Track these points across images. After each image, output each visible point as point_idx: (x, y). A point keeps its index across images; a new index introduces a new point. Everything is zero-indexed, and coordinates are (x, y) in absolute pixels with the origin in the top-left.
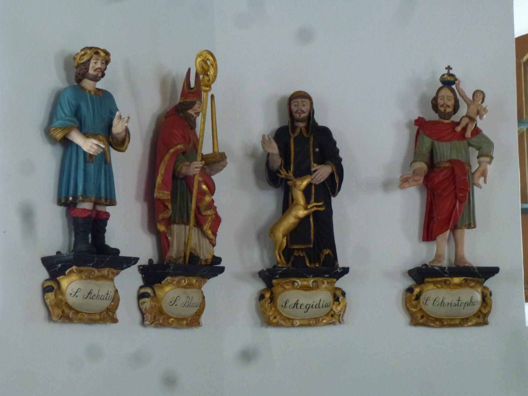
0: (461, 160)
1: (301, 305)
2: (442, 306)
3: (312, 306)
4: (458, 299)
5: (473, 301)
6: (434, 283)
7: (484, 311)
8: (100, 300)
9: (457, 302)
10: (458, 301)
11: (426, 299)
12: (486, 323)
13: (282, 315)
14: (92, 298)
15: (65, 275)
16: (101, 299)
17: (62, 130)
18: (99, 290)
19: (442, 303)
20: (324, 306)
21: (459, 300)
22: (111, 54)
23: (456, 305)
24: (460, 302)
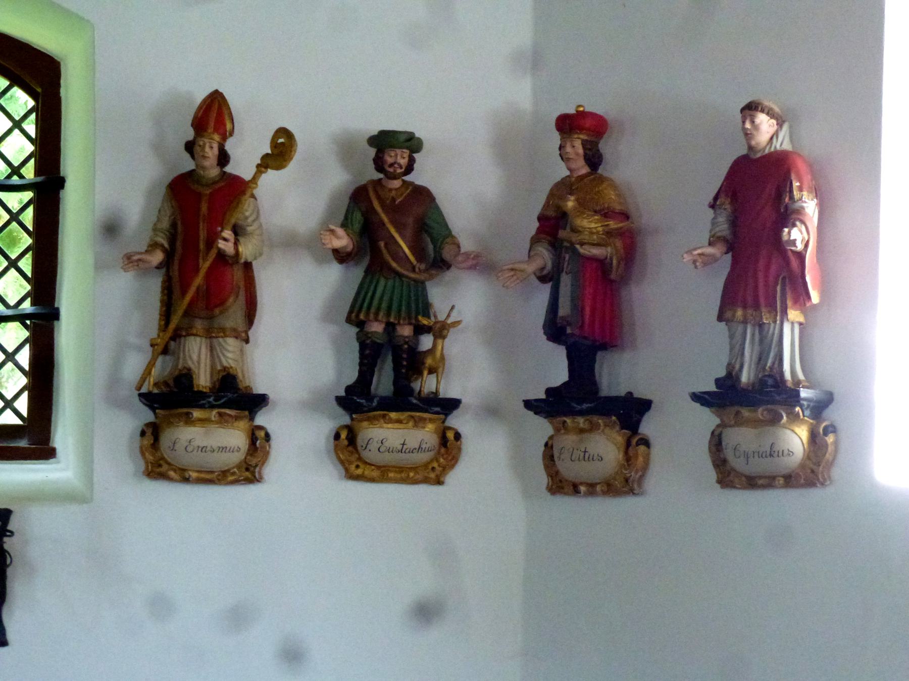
0: (716, 417)
1: (369, 441)
2: (219, 453)
3: (424, 450)
4: (402, 443)
5: (776, 448)
6: (369, 419)
7: (253, 462)
8: (592, 461)
9: (400, 447)
10: (402, 446)
11: (367, 442)
12: (439, 482)
13: (94, 105)
14: (762, 456)
15: (8, 566)
16: (579, 461)
17: (601, 226)
18: (747, 464)
19: (419, 449)
20: (426, 450)
21: (403, 444)
22: (184, 143)
23: (399, 451)
24: (405, 447)
